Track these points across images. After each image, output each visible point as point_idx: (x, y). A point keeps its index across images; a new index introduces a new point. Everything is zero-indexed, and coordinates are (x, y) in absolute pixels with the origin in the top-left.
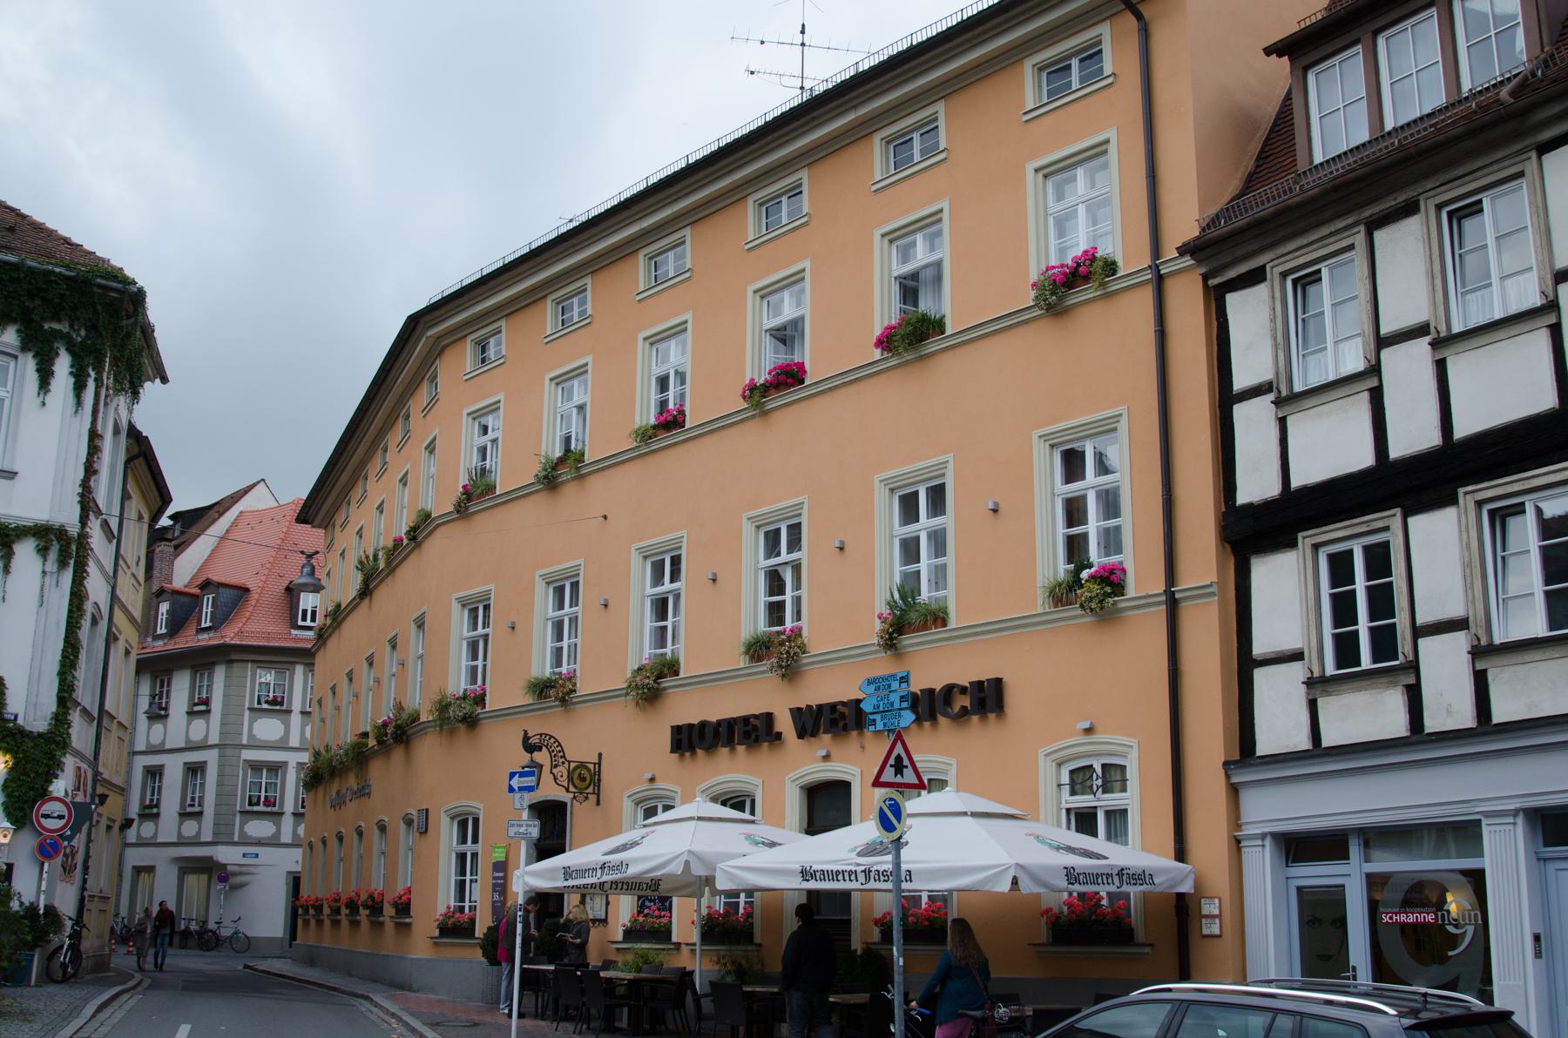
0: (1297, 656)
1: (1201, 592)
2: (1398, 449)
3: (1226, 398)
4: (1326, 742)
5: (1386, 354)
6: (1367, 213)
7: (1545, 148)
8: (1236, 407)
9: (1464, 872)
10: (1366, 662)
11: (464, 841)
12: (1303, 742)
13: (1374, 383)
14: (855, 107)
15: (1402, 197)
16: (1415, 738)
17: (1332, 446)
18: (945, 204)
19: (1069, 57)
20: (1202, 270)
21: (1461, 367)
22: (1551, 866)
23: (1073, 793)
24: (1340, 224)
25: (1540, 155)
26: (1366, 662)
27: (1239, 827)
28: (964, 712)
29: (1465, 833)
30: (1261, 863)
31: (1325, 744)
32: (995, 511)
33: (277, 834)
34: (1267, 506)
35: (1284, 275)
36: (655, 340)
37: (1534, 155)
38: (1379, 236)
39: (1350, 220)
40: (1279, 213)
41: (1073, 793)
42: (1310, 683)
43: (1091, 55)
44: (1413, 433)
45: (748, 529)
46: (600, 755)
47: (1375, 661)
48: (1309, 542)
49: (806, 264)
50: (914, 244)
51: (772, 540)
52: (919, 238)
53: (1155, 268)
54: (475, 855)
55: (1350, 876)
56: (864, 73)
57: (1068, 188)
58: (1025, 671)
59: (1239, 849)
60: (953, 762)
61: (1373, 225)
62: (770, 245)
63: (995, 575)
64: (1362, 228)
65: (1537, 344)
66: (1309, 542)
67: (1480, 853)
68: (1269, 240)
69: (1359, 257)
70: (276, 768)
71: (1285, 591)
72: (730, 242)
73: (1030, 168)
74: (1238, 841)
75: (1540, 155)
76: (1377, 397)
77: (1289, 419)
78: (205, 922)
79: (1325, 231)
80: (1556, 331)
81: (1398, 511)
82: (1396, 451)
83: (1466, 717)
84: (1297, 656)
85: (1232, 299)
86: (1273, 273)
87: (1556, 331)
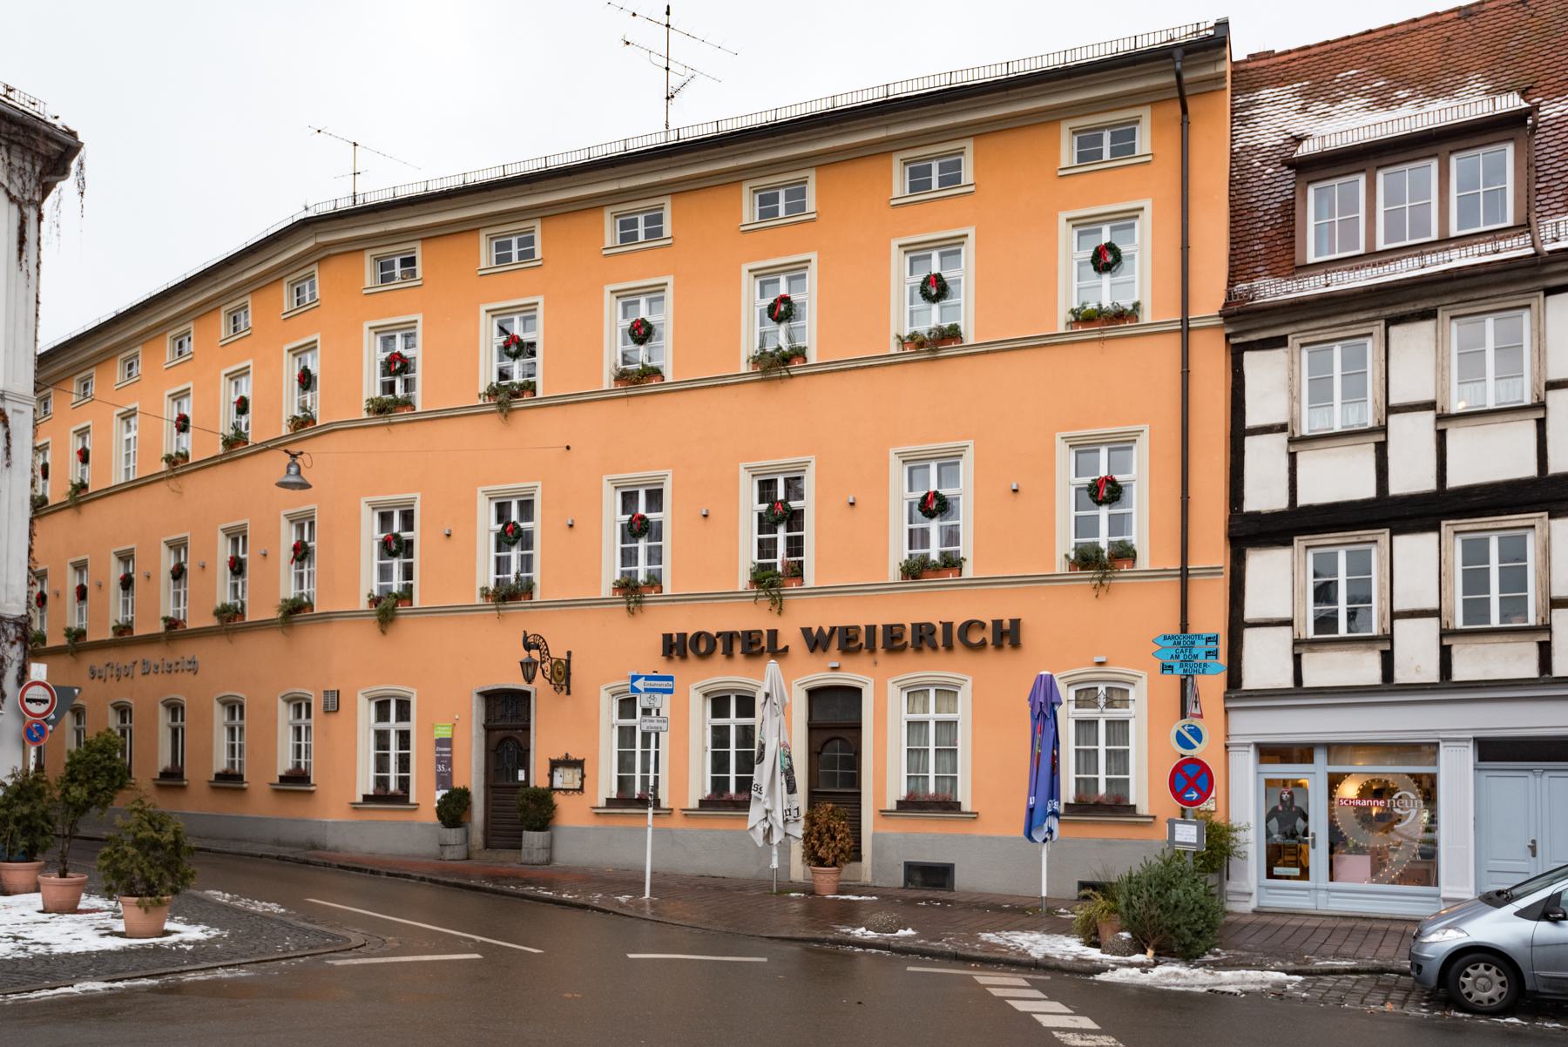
0: (1289, 623)
1: (1213, 571)
2: (1396, 488)
3: (1238, 433)
4: (1307, 683)
5: (1393, 419)
6: (1388, 312)
7: (1550, 291)
9: (1411, 775)
11: (299, 716)
12: (1287, 682)
13: (1381, 438)
14: (887, 126)
15: (1421, 306)
16: (1387, 687)
17: (1339, 478)
18: (419, 317)
19: (1103, 128)
20: (1229, 330)
21: (1308, 461)
22: (1484, 774)
23: (1077, 706)
24: (1362, 316)
26: (1343, 631)
27: (1227, 736)
29: (1427, 749)
31: (1306, 685)
32: (1015, 491)
39: (1371, 315)
41: (1077, 706)
42: (1297, 643)
44: (1412, 474)
46: (569, 653)
47: (1316, 633)
48: (1304, 544)
49: (813, 256)
51: (386, 518)
53: (1185, 320)
54: (308, 728)
55: (1313, 777)
58: (1043, 617)
59: (1227, 753)
60: (970, 680)
62: (940, 203)
63: (1017, 533)
64: (1383, 323)
66: (1304, 544)
67: (1435, 763)
68: (1278, 321)
69: (1372, 347)
71: (1275, 579)
76: (1541, 424)
77: (1299, 457)
79: (1354, 317)
81: (1387, 531)
82: (1302, 500)
83: (1432, 674)
85: (1250, 358)
87: (1541, 424)
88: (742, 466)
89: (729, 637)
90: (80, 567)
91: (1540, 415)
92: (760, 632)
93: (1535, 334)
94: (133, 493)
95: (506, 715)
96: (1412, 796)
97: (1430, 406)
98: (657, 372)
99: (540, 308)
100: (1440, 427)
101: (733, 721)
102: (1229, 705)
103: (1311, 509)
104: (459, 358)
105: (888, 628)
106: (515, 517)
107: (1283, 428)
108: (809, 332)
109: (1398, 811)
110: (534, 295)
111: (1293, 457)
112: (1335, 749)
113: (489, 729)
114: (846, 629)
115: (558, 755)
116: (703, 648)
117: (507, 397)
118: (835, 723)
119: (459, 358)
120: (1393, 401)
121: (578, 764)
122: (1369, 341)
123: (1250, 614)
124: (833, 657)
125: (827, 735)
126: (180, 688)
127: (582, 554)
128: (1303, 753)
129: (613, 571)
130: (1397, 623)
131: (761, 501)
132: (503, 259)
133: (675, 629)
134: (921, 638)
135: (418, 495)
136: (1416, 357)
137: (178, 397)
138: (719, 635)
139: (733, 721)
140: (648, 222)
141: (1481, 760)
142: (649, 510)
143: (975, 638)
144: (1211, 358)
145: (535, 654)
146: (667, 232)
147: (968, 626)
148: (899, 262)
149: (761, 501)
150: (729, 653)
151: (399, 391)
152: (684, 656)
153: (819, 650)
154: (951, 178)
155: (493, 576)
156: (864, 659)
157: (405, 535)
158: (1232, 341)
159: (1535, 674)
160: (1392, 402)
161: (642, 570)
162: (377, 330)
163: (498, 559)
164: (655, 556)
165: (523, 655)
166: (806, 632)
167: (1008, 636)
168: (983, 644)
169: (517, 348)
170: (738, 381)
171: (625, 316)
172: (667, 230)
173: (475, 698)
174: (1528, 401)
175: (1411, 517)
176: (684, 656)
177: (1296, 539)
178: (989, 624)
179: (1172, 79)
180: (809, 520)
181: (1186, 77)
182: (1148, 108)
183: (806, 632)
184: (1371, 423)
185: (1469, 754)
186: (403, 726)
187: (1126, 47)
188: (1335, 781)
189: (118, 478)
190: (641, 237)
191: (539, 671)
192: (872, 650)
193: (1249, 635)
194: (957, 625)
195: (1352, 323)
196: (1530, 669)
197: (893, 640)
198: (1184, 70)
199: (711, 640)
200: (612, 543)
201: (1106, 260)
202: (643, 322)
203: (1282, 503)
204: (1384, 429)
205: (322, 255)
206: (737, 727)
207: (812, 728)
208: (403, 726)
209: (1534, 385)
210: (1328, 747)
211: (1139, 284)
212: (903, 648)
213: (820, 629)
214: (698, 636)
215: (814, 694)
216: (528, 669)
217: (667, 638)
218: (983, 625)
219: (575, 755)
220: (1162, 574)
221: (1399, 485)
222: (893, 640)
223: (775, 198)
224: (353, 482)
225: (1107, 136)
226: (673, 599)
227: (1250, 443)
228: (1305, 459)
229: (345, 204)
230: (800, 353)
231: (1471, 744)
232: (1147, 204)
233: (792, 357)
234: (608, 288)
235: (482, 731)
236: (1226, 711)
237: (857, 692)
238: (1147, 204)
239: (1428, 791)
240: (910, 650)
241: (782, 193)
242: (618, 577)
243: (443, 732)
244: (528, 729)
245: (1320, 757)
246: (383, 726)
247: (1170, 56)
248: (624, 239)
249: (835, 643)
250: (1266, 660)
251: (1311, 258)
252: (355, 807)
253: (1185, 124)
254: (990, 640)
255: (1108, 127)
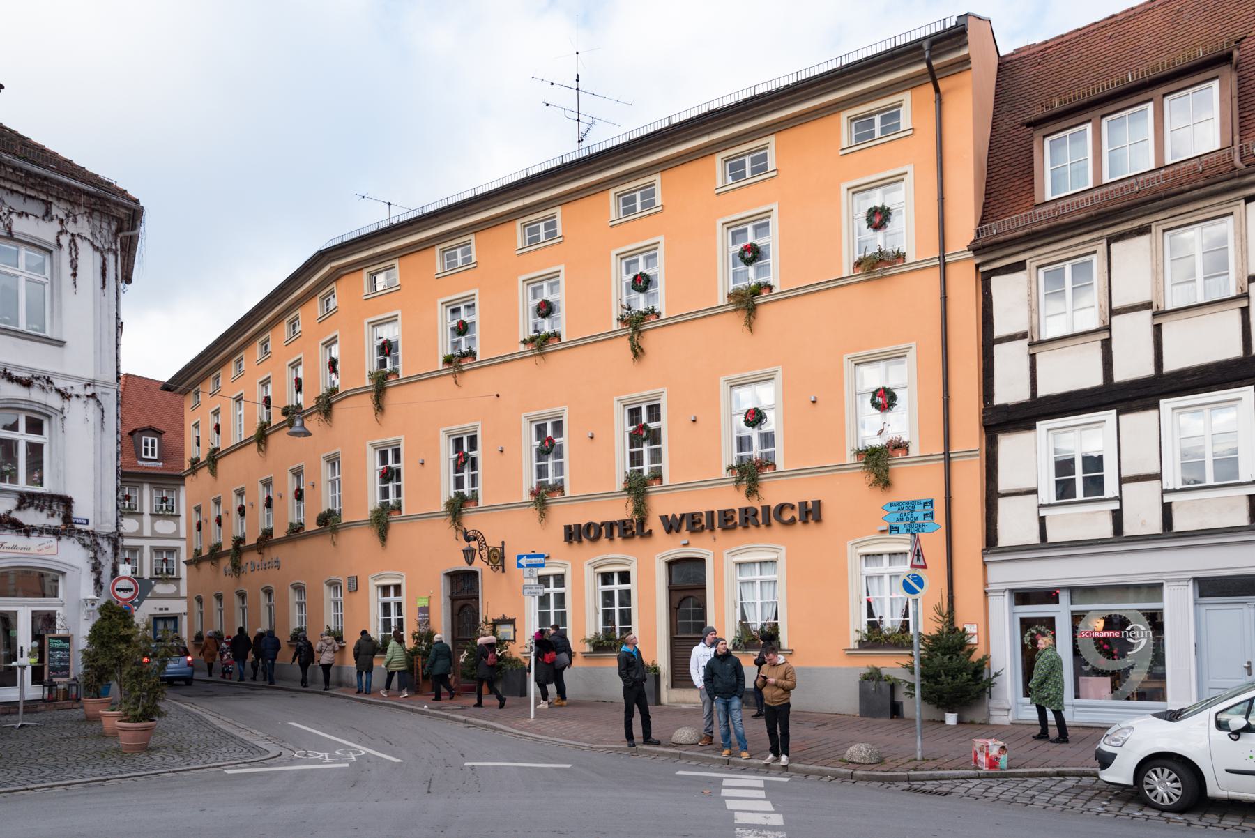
1: (969, 454)
2: (1119, 376)
3: (988, 342)
5: (1115, 319)
6: (1109, 231)
8: (996, 347)
10: (1080, 495)
12: (1035, 539)
14: (709, 134)
15: (1137, 223)
16: (1117, 539)
17: (1074, 371)
18: (562, 267)
19: (874, 114)
20: (978, 261)
25: (1246, 203)
26: (1080, 495)
28: (793, 521)
29: (1155, 589)
30: (1002, 608)
31: (1049, 540)
33: (178, 591)
34: (1019, 406)
35: (1038, 267)
36: (375, 324)
37: (1243, 202)
38: (1115, 247)
40: (1027, 235)
43: (891, 116)
44: (1133, 364)
45: (525, 423)
49: (661, 239)
50: (542, 287)
51: (384, 455)
52: (545, 284)
53: (942, 257)
56: (715, 111)
57: (632, 266)
60: (635, 559)
61: (1111, 240)
62: (762, 184)
64: (1105, 241)
65: (1232, 318)
67: (1161, 600)
69: (1098, 262)
70: (172, 551)
72: (596, 221)
73: (719, 222)
74: (986, 593)
75: (1246, 203)
77: (1038, 356)
78: (430, 635)
80: (1245, 311)
81: (1114, 412)
82: (1041, 393)
83: (1156, 527)
84: (1034, 492)
85: (995, 281)
86: (1031, 265)
87: (1245, 311)
88: (615, 399)
89: (611, 525)
90: (240, 493)
91: (1244, 304)
92: (733, 511)
93: (1238, 237)
94: (243, 450)
95: (463, 587)
96: (1142, 628)
97: (1147, 306)
98: (900, 256)
99: (562, 275)
100: (1156, 322)
101: (616, 586)
102: (986, 559)
103: (1049, 399)
104: (504, 322)
105: (724, 513)
106: (644, 419)
107: (1024, 335)
108: (774, 272)
109: (1130, 640)
110: (470, 288)
111: (1033, 358)
112: (1079, 592)
113: (453, 599)
114: (693, 515)
115: (498, 616)
116: (592, 534)
117: (457, 362)
118: (687, 584)
119: (504, 322)
120: (1116, 304)
121: (512, 622)
122: (1094, 258)
123: (1003, 485)
124: (685, 535)
125: (682, 595)
126: (270, 578)
127: (509, 473)
128: (1049, 596)
129: (530, 480)
130: (1124, 486)
131: (631, 424)
132: (534, 240)
133: (573, 522)
134: (747, 519)
135: (402, 437)
136: (1134, 265)
137: (265, 383)
138: (603, 524)
139: (616, 586)
140: (547, 227)
141: (1201, 596)
142: (650, 419)
143: (787, 516)
144: (964, 281)
145: (474, 545)
146: (658, 202)
147: (782, 508)
148: (522, 289)
149: (631, 424)
150: (610, 536)
151: (389, 367)
152: (580, 541)
153: (674, 532)
154: (760, 168)
155: (535, 480)
156: (706, 536)
157: (652, 425)
158: (981, 269)
159: (1160, 531)
160: (1114, 306)
161: (467, 490)
162: (728, 225)
163: (632, 454)
164: (656, 456)
165: (465, 545)
166: (664, 519)
167: (574, 534)
168: (793, 521)
169: (546, 309)
170: (433, 376)
171: (628, 272)
172: (659, 200)
173: (442, 577)
174: (1233, 294)
175: (1135, 399)
176: (580, 541)
177: (1038, 424)
178: (797, 506)
179: (924, 66)
180: (664, 436)
181: (934, 63)
182: (909, 93)
183: (664, 519)
184: (1095, 325)
185: (1189, 591)
186: (398, 599)
187: (791, 80)
188: (1077, 618)
189: (235, 441)
190: (542, 239)
191: (477, 556)
192: (712, 529)
193: (1002, 503)
194: (773, 507)
195: (1079, 244)
196: (1106, 530)
197: (727, 521)
198: (935, 56)
199: (599, 529)
200: (529, 463)
201: (879, 218)
202: (643, 275)
203: (1025, 396)
204: (1108, 328)
205: (336, 276)
206: (555, 594)
207: (672, 590)
208: (398, 599)
209: (1238, 279)
210: (1072, 590)
211: (903, 235)
212: (734, 527)
213: (674, 516)
214: (589, 525)
215: (671, 564)
216: (469, 554)
217: (568, 528)
218: (793, 507)
219: (509, 616)
220: (929, 458)
221: (1122, 374)
222: (727, 521)
223: (633, 200)
224: (425, 422)
225: (877, 119)
226: (675, 488)
227: (998, 349)
228: (1042, 359)
229: (384, 225)
230: (557, 335)
231: (1191, 583)
232: (909, 168)
233: (645, 314)
234: (521, 279)
235: (449, 602)
236: (985, 564)
237: (701, 561)
238: (909, 168)
239: (1155, 621)
240: (799, 523)
241: (638, 194)
242: (534, 485)
243: (423, 602)
244: (477, 598)
245: (1064, 598)
246: (386, 599)
247: (920, 47)
248: (626, 212)
249: (684, 526)
250: (1016, 523)
251: (1049, 197)
252: (849, 652)
253: (940, 102)
254: (797, 517)
255: (879, 113)
